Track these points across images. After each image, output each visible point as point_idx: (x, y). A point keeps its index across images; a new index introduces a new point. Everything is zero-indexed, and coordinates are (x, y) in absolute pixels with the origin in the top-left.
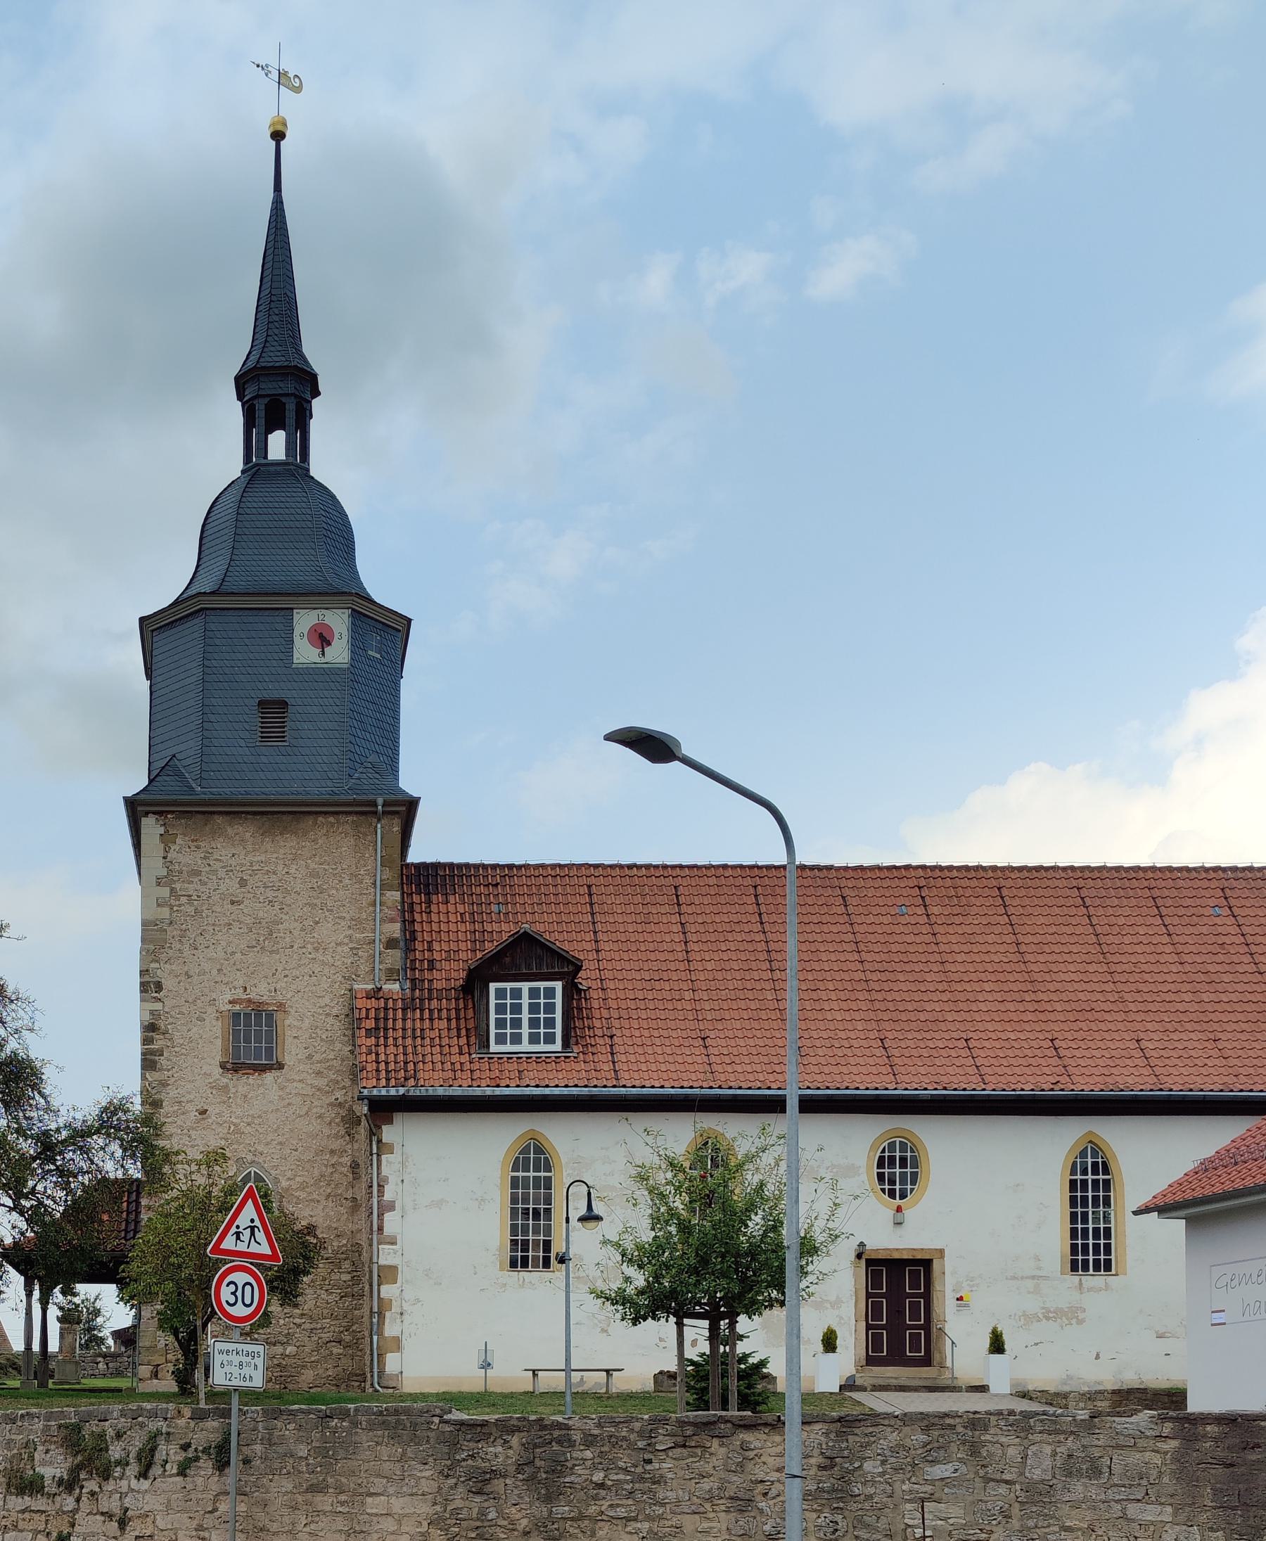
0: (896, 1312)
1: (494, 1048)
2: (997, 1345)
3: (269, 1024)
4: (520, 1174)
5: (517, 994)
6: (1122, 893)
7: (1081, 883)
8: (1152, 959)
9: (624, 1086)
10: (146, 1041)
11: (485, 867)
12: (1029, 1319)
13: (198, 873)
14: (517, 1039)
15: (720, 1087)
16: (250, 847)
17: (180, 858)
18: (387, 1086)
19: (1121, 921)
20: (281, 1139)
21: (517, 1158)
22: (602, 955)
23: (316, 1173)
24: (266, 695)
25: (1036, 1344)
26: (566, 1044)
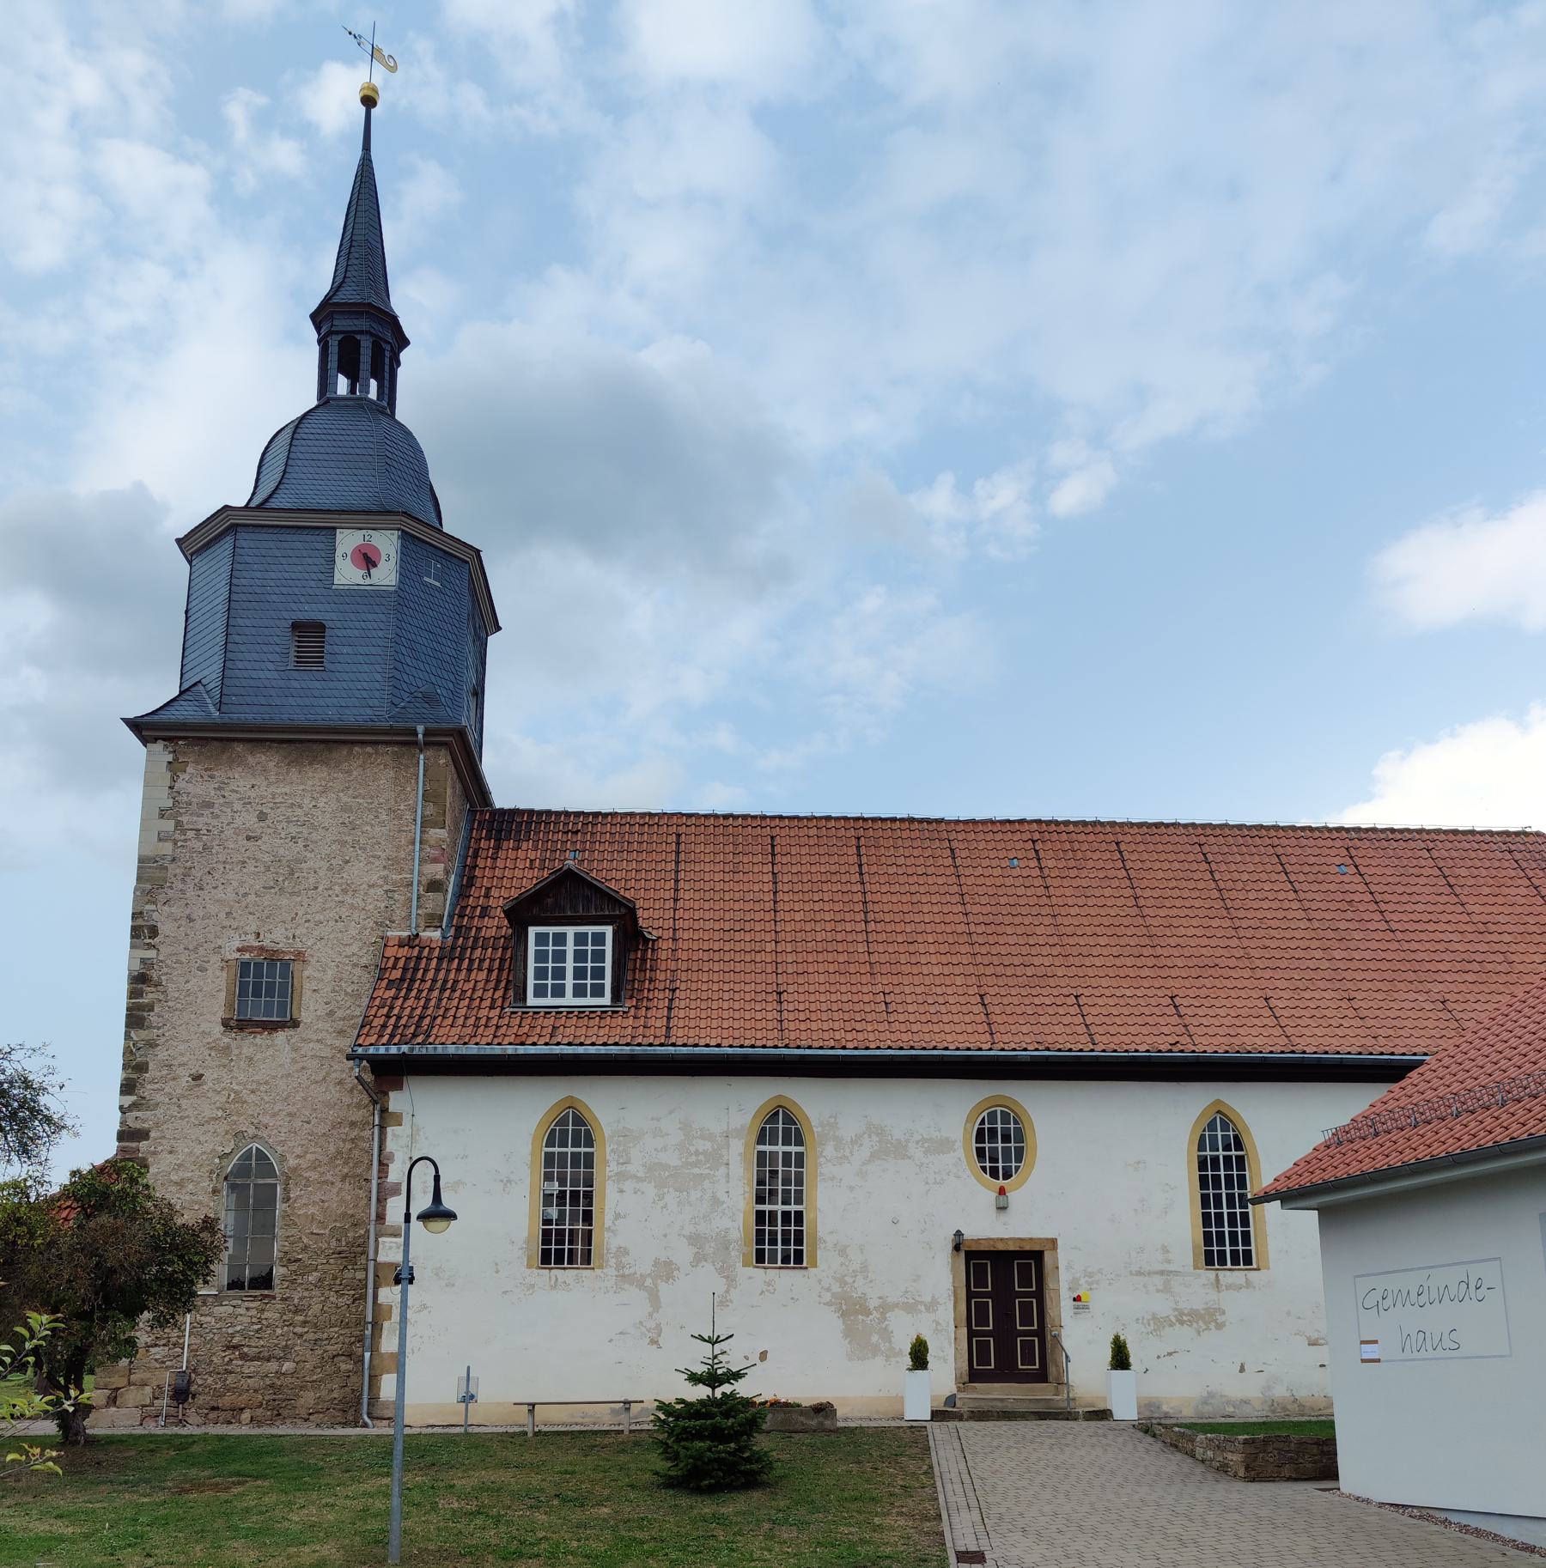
0: (1005, 1316)
1: (531, 1000)
2: (1120, 1359)
3: (284, 975)
4: (556, 1150)
5: (560, 939)
6: (1244, 850)
7: (1203, 840)
8: (1279, 914)
9: (673, 1045)
10: (133, 994)
11: (567, 814)
12: (1158, 1324)
13: (209, 805)
14: (559, 991)
15: (786, 1046)
16: (273, 778)
17: (190, 788)
18: (389, 1043)
19: (1245, 877)
20: (291, 1109)
21: (553, 1131)
22: (680, 904)
23: (332, 1149)
24: (301, 616)
25: (1170, 1354)
26: (616, 996)
